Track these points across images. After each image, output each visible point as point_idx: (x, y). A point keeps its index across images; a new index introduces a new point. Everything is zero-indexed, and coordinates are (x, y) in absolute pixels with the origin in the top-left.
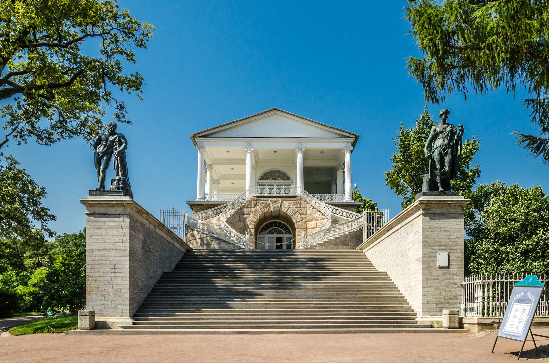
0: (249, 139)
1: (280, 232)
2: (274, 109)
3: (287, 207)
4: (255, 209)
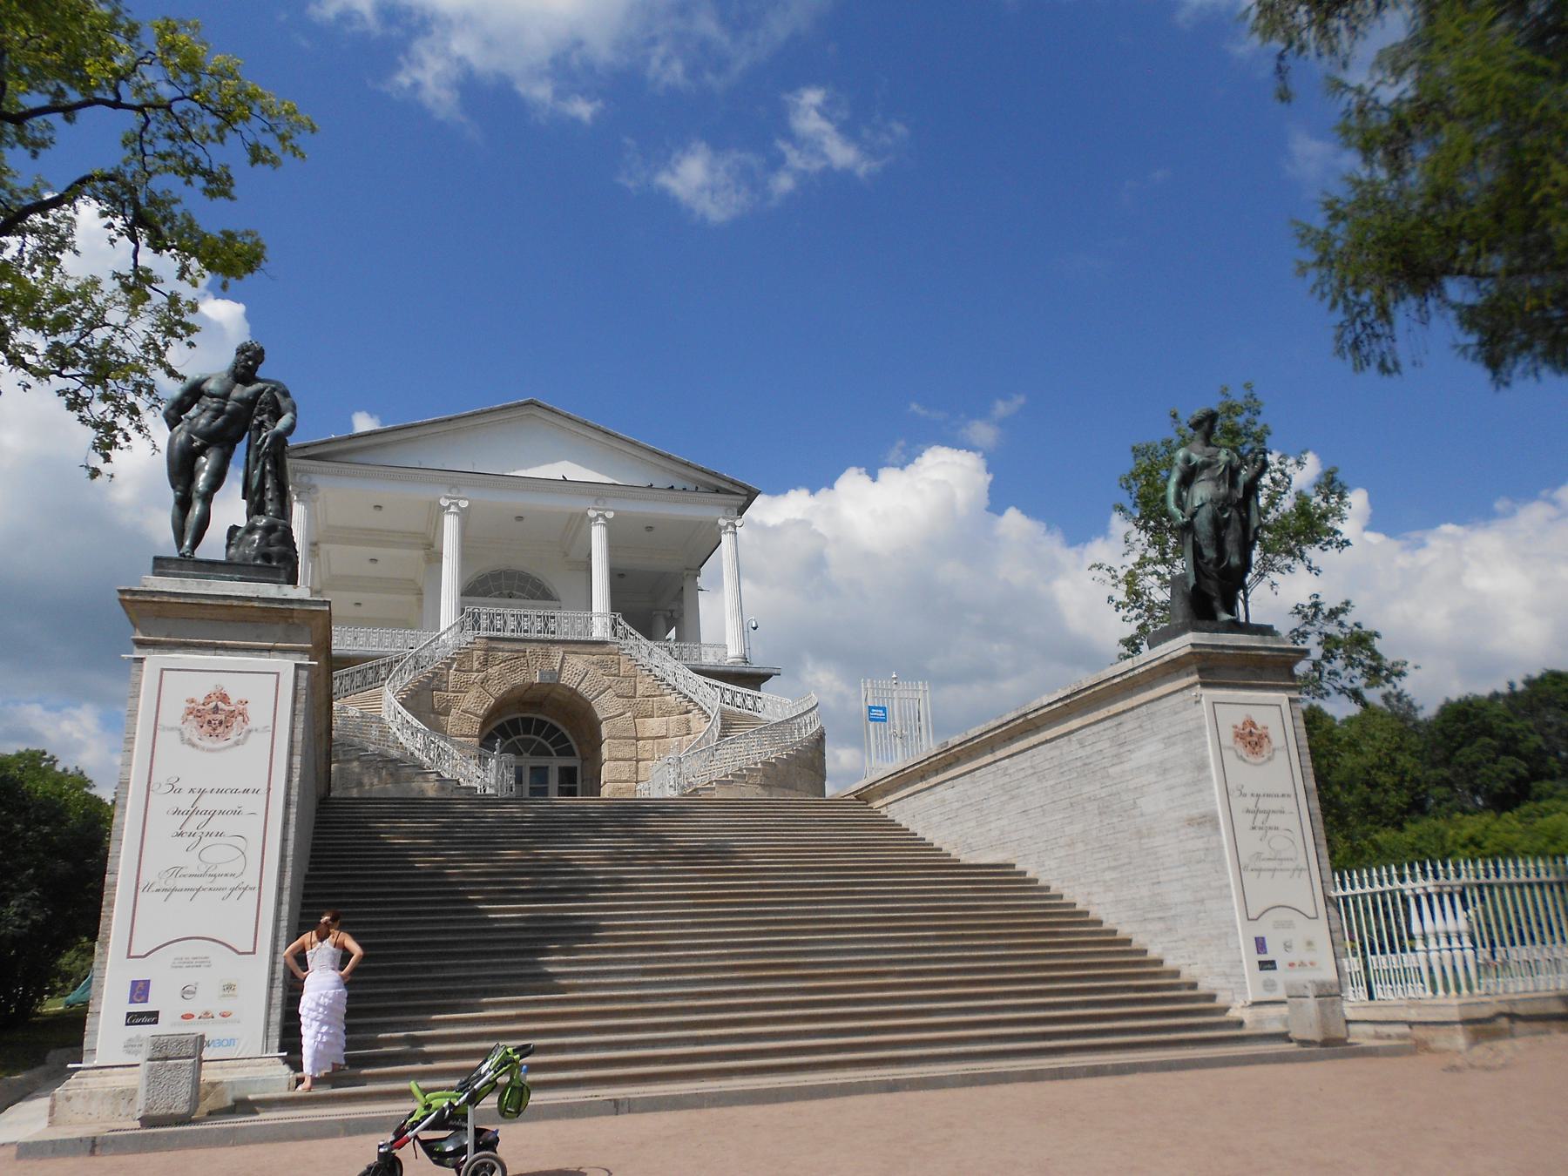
0: (455, 478)
1: (542, 752)
2: (531, 403)
3: (575, 672)
4: (482, 675)
